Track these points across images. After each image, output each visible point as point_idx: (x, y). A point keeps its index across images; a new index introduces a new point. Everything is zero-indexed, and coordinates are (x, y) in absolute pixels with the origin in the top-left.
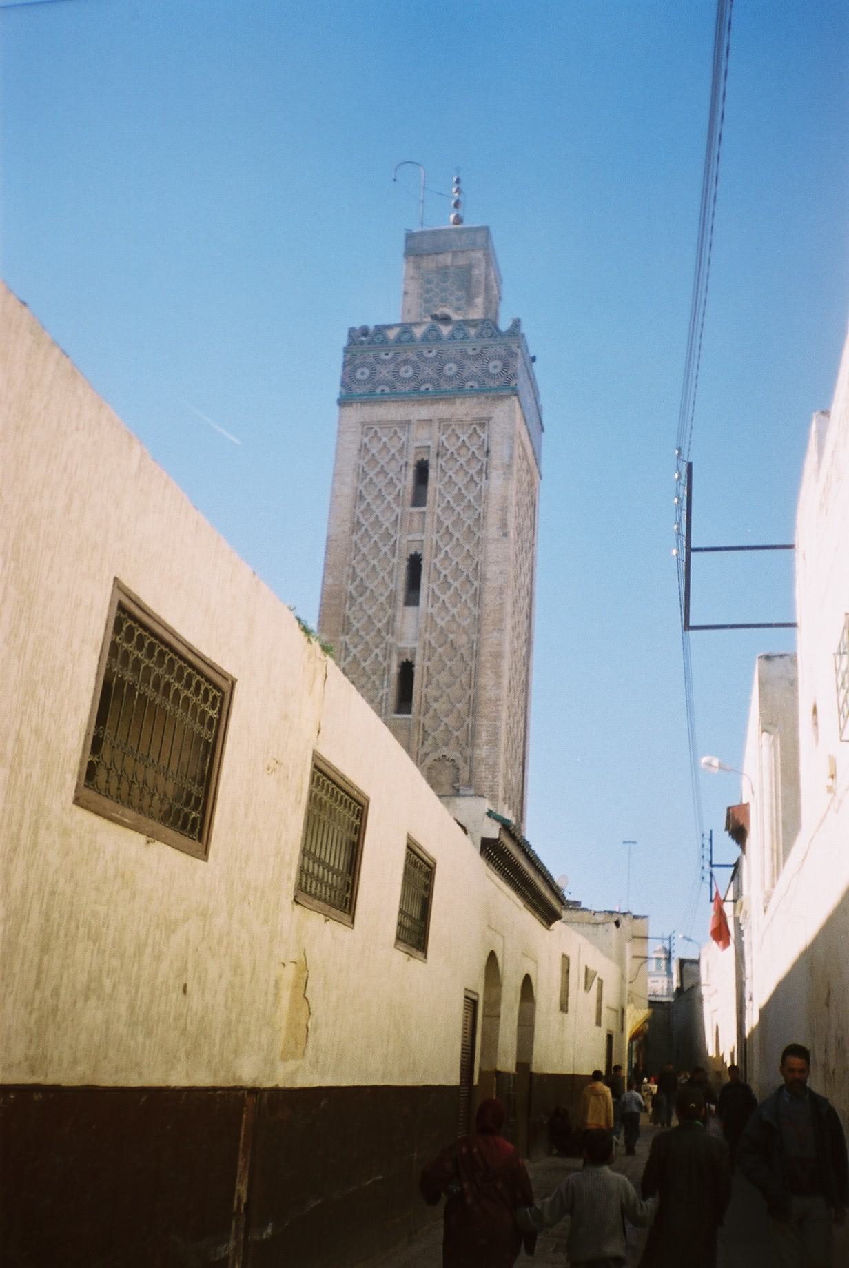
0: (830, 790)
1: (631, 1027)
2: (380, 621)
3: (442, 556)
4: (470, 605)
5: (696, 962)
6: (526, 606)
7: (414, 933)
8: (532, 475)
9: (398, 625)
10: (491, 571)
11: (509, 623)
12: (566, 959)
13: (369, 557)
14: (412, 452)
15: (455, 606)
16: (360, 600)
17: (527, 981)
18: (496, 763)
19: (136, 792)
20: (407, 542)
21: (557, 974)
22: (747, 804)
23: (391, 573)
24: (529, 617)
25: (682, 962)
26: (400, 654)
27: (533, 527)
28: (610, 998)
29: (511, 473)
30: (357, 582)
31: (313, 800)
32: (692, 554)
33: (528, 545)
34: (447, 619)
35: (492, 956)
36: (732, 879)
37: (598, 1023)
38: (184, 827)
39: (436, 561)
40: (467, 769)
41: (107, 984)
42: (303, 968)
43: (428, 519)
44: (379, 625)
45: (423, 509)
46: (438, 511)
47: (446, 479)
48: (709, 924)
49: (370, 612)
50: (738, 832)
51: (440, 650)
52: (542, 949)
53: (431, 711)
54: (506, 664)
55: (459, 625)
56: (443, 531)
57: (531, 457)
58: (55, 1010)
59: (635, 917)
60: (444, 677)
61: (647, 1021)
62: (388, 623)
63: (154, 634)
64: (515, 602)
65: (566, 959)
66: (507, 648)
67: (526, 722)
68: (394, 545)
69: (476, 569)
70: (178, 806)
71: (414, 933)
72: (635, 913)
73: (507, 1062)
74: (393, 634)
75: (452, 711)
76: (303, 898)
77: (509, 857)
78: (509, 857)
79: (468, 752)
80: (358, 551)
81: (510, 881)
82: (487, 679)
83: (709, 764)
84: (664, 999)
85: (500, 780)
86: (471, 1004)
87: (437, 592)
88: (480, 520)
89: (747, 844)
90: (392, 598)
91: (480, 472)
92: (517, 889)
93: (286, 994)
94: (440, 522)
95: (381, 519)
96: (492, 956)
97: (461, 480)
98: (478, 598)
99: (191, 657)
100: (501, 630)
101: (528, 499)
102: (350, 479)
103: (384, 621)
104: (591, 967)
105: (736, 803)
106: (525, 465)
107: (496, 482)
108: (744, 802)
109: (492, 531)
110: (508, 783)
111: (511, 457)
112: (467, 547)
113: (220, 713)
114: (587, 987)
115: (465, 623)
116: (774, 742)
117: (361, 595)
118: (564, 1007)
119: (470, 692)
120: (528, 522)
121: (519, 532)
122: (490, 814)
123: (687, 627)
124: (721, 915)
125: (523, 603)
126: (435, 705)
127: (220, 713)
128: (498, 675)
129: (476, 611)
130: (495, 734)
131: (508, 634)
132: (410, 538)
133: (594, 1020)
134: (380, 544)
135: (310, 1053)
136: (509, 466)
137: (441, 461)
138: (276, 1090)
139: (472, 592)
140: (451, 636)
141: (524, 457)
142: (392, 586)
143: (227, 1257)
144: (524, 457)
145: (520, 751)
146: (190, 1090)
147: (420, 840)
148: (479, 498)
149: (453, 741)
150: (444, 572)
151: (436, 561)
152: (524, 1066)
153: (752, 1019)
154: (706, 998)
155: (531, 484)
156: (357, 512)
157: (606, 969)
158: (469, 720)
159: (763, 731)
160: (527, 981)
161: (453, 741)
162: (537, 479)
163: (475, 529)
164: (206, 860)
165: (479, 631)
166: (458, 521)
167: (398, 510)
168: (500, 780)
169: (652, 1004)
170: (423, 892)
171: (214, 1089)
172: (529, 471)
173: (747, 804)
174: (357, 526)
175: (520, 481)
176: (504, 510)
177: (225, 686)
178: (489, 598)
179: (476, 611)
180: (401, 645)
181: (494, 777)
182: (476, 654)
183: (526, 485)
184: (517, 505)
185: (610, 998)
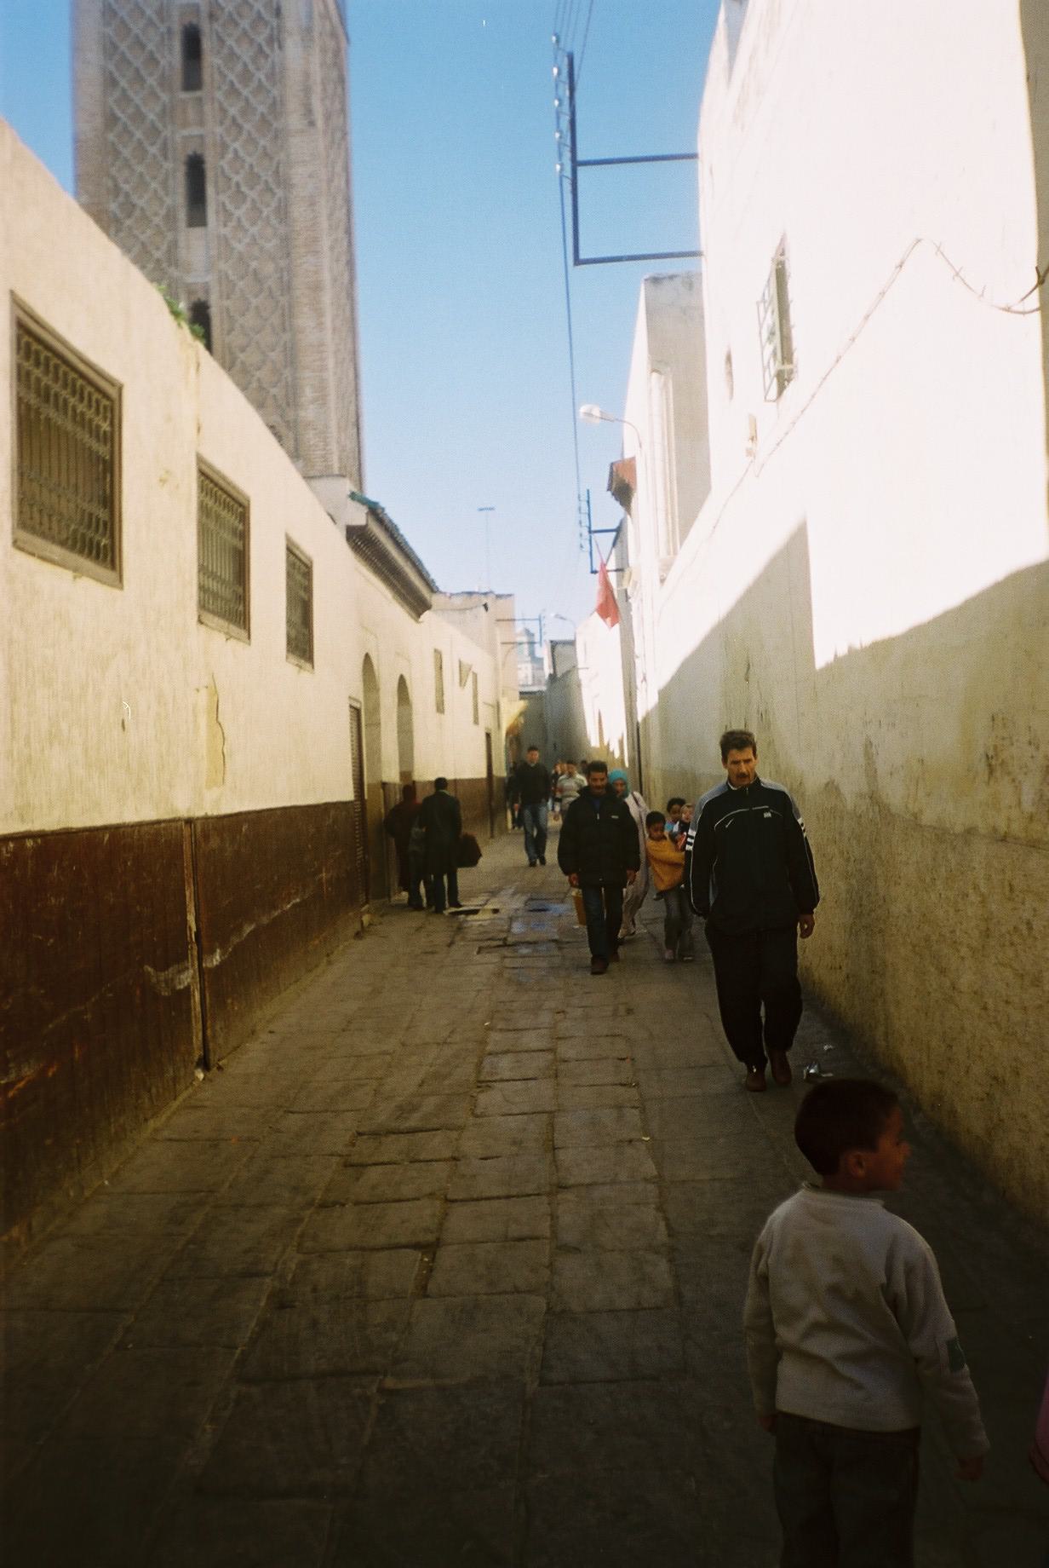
0: (749, 452)
1: (506, 724)
2: (158, 249)
3: (230, 156)
4: (274, 221)
5: (572, 643)
6: (344, 218)
7: (301, 644)
8: (338, 43)
9: (182, 253)
10: (298, 174)
11: (326, 243)
12: (438, 655)
13: (133, 162)
14: (176, 14)
15: (254, 224)
16: (128, 222)
17: (402, 681)
18: (326, 426)
19: (55, 526)
20: (183, 137)
21: (431, 671)
22: (633, 459)
23: (164, 184)
24: (349, 232)
25: (554, 645)
26: (190, 293)
27: (343, 111)
28: (485, 695)
29: (312, 40)
30: (121, 199)
31: (203, 509)
32: (580, 170)
33: (338, 135)
34: (247, 240)
35: (367, 656)
36: (614, 544)
37: (476, 722)
38: (98, 557)
39: (223, 163)
40: (291, 435)
41: (64, 726)
42: (213, 691)
43: (207, 108)
44: (157, 254)
45: (198, 94)
46: (219, 95)
47: (225, 51)
48: (594, 597)
49: (143, 237)
50: (623, 491)
51: (241, 283)
52: (411, 645)
53: (238, 362)
54: (327, 298)
55: (261, 249)
56: (228, 122)
57: (335, 19)
58: (29, 760)
59: (499, 596)
60: (249, 320)
61: (522, 714)
62: (169, 251)
63: (48, 347)
64: (331, 215)
65: (438, 655)
66: (326, 277)
67: (356, 369)
68: (165, 144)
69: (277, 172)
70: (82, 530)
71: (301, 644)
72: (498, 592)
73: (392, 775)
74: (177, 266)
75: (264, 362)
76: (208, 617)
77: (377, 545)
78: (377, 545)
79: (291, 415)
80: (117, 153)
81: (378, 571)
82: (305, 320)
83: (589, 414)
84: (535, 689)
85: (334, 447)
86: (356, 712)
87: (230, 207)
88: (277, 107)
89: (633, 505)
90: (170, 218)
91: (270, 40)
92: (386, 580)
93: (203, 721)
94: (223, 111)
95: (144, 109)
96: (367, 656)
97: (245, 53)
98: (283, 212)
99: (82, 367)
100: (316, 253)
101: (334, 74)
102: (94, 55)
103: (164, 247)
104: (465, 661)
105: (615, 458)
106: (328, 27)
107: (293, 49)
108: (627, 456)
109: (294, 121)
110: (343, 449)
111: (310, 17)
112: (262, 142)
113: (112, 424)
114: (462, 683)
115: (269, 246)
116: (665, 385)
117: (129, 216)
118: (440, 708)
119: (286, 337)
120: (337, 106)
121: (328, 117)
122: (353, 496)
123: (578, 261)
124: (606, 585)
125: (341, 214)
126: (242, 356)
127: (112, 424)
128: (319, 313)
129: (282, 230)
130: (322, 388)
131: (326, 261)
132: (185, 132)
133: (472, 719)
134: (146, 144)
135: (229, 778)
136: (309, 30)
137: (216, 26)
138: (206, 818)
139: (274, 204)
140: (254, 264)
141: (326, 16)
142: (168, 201)
143: (188, 988)
144: (326, 16)
145: (352, 408)
146: (140, 825)
147: (297, 538)
148: (271, 76)
149: (270, 402)
150: (236, 178)
151: (223, 163)
152: (406, 775)
153: (647, 702)
154: (584, 683)
155: (337, 53)
156: (111, 100)
157: (480, 661)
158: (287, 373)
159: (654, 371)
160: (402, 681)
161: (270, 402)
162: (343, 44)
163: (270, 118)
164: (121, 588)
165: (288, 255)
166: (247, 110)
167: (165, 97)
168: (334, 447)
169: (523, 695)
170: (302, 593)
171: (158, 822)
172: (334, 35)
173: (633, 459)
174: (111, 120)
175: (324, 51)
176: (307, 91)
177: (112, 392)
178: (298, 211)
179: (282, 230)
180: (190, 279)
181: (326, 444)
182: (287, 288)
183: (330, 55)
184: (323, 83)
185: (485, 695)
